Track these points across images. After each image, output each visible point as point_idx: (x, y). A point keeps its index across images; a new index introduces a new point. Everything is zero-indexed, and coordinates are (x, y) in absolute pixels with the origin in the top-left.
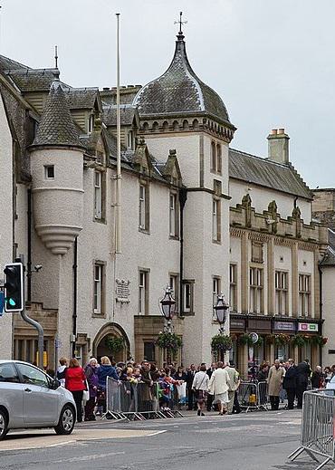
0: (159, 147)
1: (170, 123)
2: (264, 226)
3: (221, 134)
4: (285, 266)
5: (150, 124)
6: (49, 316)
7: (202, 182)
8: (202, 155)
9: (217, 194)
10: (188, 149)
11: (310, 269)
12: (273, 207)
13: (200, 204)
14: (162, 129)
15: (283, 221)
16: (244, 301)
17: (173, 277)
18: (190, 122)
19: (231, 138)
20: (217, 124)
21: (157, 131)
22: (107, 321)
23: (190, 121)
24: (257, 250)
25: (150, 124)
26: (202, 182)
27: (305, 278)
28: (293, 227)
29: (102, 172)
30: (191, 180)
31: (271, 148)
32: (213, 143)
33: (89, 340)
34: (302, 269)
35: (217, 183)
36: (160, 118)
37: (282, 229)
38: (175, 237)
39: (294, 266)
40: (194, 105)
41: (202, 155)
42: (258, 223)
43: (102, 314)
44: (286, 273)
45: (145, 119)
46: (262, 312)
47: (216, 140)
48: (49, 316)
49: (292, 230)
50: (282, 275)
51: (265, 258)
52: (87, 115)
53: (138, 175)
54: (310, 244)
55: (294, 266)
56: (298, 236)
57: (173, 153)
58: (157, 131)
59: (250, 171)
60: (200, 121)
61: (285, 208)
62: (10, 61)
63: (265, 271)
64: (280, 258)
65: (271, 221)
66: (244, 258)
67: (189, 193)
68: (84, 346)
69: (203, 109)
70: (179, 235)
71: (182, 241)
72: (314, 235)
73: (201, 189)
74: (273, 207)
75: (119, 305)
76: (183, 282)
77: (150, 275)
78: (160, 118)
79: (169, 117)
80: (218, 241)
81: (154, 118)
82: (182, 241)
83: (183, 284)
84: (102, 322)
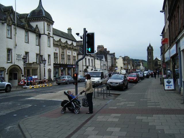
0: (34, 24)
1: (37, 19)
2: (64, 45)
3: (50, 22)
4: (70, 54)
5: (32, 19)
6: (167, 93)
7: (44, 32)
8: (44, 26)
9: (49, 36)
10: (41, 25)
11: (76, 55)
12: (67, 42)
13: (44, 38)
14: (35, 20)
15: (69, 45)
16: (60, 61)
17: (37, 55)
18: (41, 18)
19: (53, 24)
20: (49, 20)
21: (34, 21)
22: (13, 64)
23: (41, 18)
24: (63, 51)
25: (32, 19)
26: (44, 32)
27: (74, 57)
28: (71, 46)
29: (10, 26)
30: (42, 32)
31: (68, 32)
32: (48, 24)
33: (5, 69)
34: (74, 55)
35: (49, 33)
36: (34, 18)
37: (69, 46)
38: (38, 45)
39: (72, 54)
40: (42, 14)
41: (44, 26)
42: (63, 45)
43: (11, 63)
44: (70, 56)
45: (31, 18)
46: (64, 63)
47: (49, 24)
48: (167, 93)
49: (71, 47)
50: (69, 56)
51: (65, 52)
52: (24, 19)
53: (24, 29)
54: (75, 50)
55: (72, 54)
56: (73, 48)
57: (37, 25)
58: (34, 21)
59: (57, 33)
60: (44, 18)
61: (70, 42)
62: (3, 5)
63: (65, 55)
64: (69, 53)
65: (66, 45)
66: (60, 52)
67: (183, 102)
68: (4, 70)
69: (44, 15)
70: (39, 45)
71: (40, 46)
72: (76, 48)
73: (44, 34)
74: (67, 42)
75: (18, 60)
76: (40, 56)
77: (29, 54)
78: (34, 18)
79: (36, 18)
80: (50, 47)
81: (33, 18)
82: (40, 46)
83: (40, 56)
84: (11, 64)
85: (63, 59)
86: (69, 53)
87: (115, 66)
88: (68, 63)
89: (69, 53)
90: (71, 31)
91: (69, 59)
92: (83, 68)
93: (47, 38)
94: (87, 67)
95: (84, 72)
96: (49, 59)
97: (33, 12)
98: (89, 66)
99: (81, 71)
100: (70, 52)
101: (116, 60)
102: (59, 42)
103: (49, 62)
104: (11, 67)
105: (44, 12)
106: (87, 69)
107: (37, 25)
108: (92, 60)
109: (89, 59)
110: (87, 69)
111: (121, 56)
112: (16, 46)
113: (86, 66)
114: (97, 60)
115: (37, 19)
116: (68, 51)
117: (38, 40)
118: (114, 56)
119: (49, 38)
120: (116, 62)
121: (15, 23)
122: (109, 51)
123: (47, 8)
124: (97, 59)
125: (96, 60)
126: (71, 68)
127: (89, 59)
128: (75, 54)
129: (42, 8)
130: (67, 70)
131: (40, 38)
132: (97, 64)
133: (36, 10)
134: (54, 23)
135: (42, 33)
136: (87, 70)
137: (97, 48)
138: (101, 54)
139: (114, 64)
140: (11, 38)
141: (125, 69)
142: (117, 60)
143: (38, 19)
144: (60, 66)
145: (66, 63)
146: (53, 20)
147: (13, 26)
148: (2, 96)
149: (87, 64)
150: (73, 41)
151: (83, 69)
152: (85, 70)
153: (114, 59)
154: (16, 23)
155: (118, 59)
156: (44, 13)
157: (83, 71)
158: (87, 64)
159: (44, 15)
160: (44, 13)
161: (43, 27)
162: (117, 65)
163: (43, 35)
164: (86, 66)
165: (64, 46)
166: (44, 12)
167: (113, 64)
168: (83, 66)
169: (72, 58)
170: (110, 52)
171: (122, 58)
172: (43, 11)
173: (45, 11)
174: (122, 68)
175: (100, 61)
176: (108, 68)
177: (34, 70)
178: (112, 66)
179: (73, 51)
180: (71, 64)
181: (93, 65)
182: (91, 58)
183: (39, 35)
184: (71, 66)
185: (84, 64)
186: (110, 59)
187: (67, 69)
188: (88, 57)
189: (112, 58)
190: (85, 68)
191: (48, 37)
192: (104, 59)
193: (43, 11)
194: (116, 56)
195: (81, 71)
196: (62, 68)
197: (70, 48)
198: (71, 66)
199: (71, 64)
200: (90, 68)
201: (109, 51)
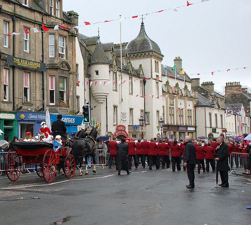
0: (136, 64)
9: (158, 81)
11: (191, 107)
13: (151, 84)
17: (142, 111)
20: (157, 54)
24: (171, 101)
29: (115, 73)
30: (147, 75)
32: (155, 61)
34: (188, 108)
35: (157, 76)
38: (142, 97)
39: (186, 106)
41: (151, 66)
46: (174, 123)
47: (157, 60)
51: (175, 104)
52: (109, 52)
53: (128, 74)
54: (191, 98)
55: (186, 106)
57: (141, 66)
60: (151, 53)
61: (182, 85)
64: (181, 104)
65: (177, 90)
76: (145, 113)
81: (133, 53)
90: (181, 64)
92: (206, 131)
97: (133, 43)
98: (217, 127)
100: (182, 101)
105: (150, 43)
109: (216, 115)
112: (122, 100)
113: (211, 127)
116: (180, 101)
117: (142, 88)
121: (120, 68)
123: (152, 35)
126: (184, 133)
127: (216, 115)
130: (178, 135)
131: (144, 84)
132: (228, 124)
133: (136, 39)
136: (213, 135)
137: (226, 87)
138: (234, 101)
140: (116, 90)
141: (69, 75)
144: (168, 128)
145: (177, 124)
147: (118, 73)
148: (7, 199)
152: (209, 135)
154: (122, 68)
158: (214, 125)
159: (151, 48)
160: (151, 45)
164: (211, 127)
166: (150, 43)
168: (206, 128)
172: (149, 41)
173: (152, 42)
179: (188, 100)
184: (184, 129)
185: (208, 125)
187: (178, 133)
190: (209, 131)
191: (156, 82)
192: (242, 112)
196: (172, 133)
198: (184, 129)
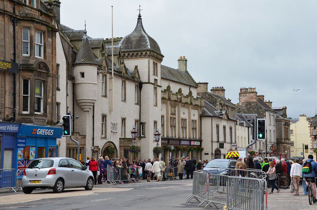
0: (130, 64)
1: (135, 53)
2: (176, 99)
4: (185, 116)
5: (126, 54)
7: (149, 79)
8: (149, 68)
9: (155, 85)
11: (196, 118)
13: (148, 90)
15: (184, 97)
17: (136, 121)
19: (162, 60)
21: (130, 57)
23: (144, 53)
24: (173, 110)
25: (126, 54)
26: (149, 79)
27: (194, 121)
28: (189, 99)
30: (144, 79)
32: (154, 63)
33: (99, 149)
34: (193, 118)
35: (156, 80)
36: (131, 52)
37: (184, 100)
39: (189, 116)
41: (149, 68)
42: (173, 98)
43: (105, 138)
44: (186, 120)
45: (124, 52)
46: (175, 136)
47: (155, 62)
49: (188, 100)
50: (184, 120)
51: (177, 113)
52: (99, 50)
54: (196, 107)
55: (189, 116)
56: (191, 104)
57: (136, 67)
58: (130, 57)
61: (185, 91)
64: (184, 113)
65: (179, 97)
66: (167, 113)
68: (97, 151)
70: (139, 103)
71: (140, 105)
72: (198, 103)
73: (149, 83)
76: (141, 123)
78: (131, 52)
79: (135, 51)
81: (128, 52)
82: (140, 105)
83: (141, 124)
85: (173, 126)
86: (184, 113)
87: (287, 141)
88: (170, 136)
89: (184, 113)
91: (184, 128)
92: (212, 146)
93: (153, 87)
94: (222, 146)
95: (214, 156)
96: (104, 125)
98: (225, 142)
99: (208, 154)
100: (186, 110)
101: (289, 125)
102: (167, 92)
103: (102, 130)
104: (106, 145)
106: (221, 150)
107: (136, 67)
108: (231, 128)
109: (224, 127)
110: (221, 150)
111: (303, 115)
114: (240, 127)
115: (135, 53)
118: (285, 115)
119: (155, 88)
120: (288, 132)
122: (270, 103)
124: (241, 124)
125: (238, 127)
127: (224, 127)
128: (195, 115)
129: (144, 34)
131: (140, 89)
134: (164, 59)
135: (143, 82)
136: (220, 151)
137: (240, 94)
139: (283, 136)
142: (292, 126)
143: (137, 54)
146: (162, 53)
149: (221, 139)
150: (190, 86)
151: (212, 150)
152: (216, 151)
153: (283, 123)
155: (296, 121)
156: (149, 43)
157: (212, 154)
158: (221, 139)
161: (147, 70)
162: (292, 138)
163: (145, 84)
164: (218, 142)
165: (175, 101)
167: (281, 136)
168: (212, 142)
169: (179, 123)
170: (274, 106)
171: (308, 119)
172: (146, 36)
174: (307, 147)
175: (247, 129)
176: (268, 148)
177: (73, 150)
178: (279, 142)
180: (177, 137)
181: (233, 141)
182: (228, 125)
183: (140, 86)
185: (215, 139)
186: (273, 122)
188: (222, 121)
189: (277, 121)
190: (216, 146)
193: (147, 38)
194: (289, 114)
195: (208, 154)
197: (186, 103)
199: (177, 137)
200: (227, 146)
201: (270, 103)
